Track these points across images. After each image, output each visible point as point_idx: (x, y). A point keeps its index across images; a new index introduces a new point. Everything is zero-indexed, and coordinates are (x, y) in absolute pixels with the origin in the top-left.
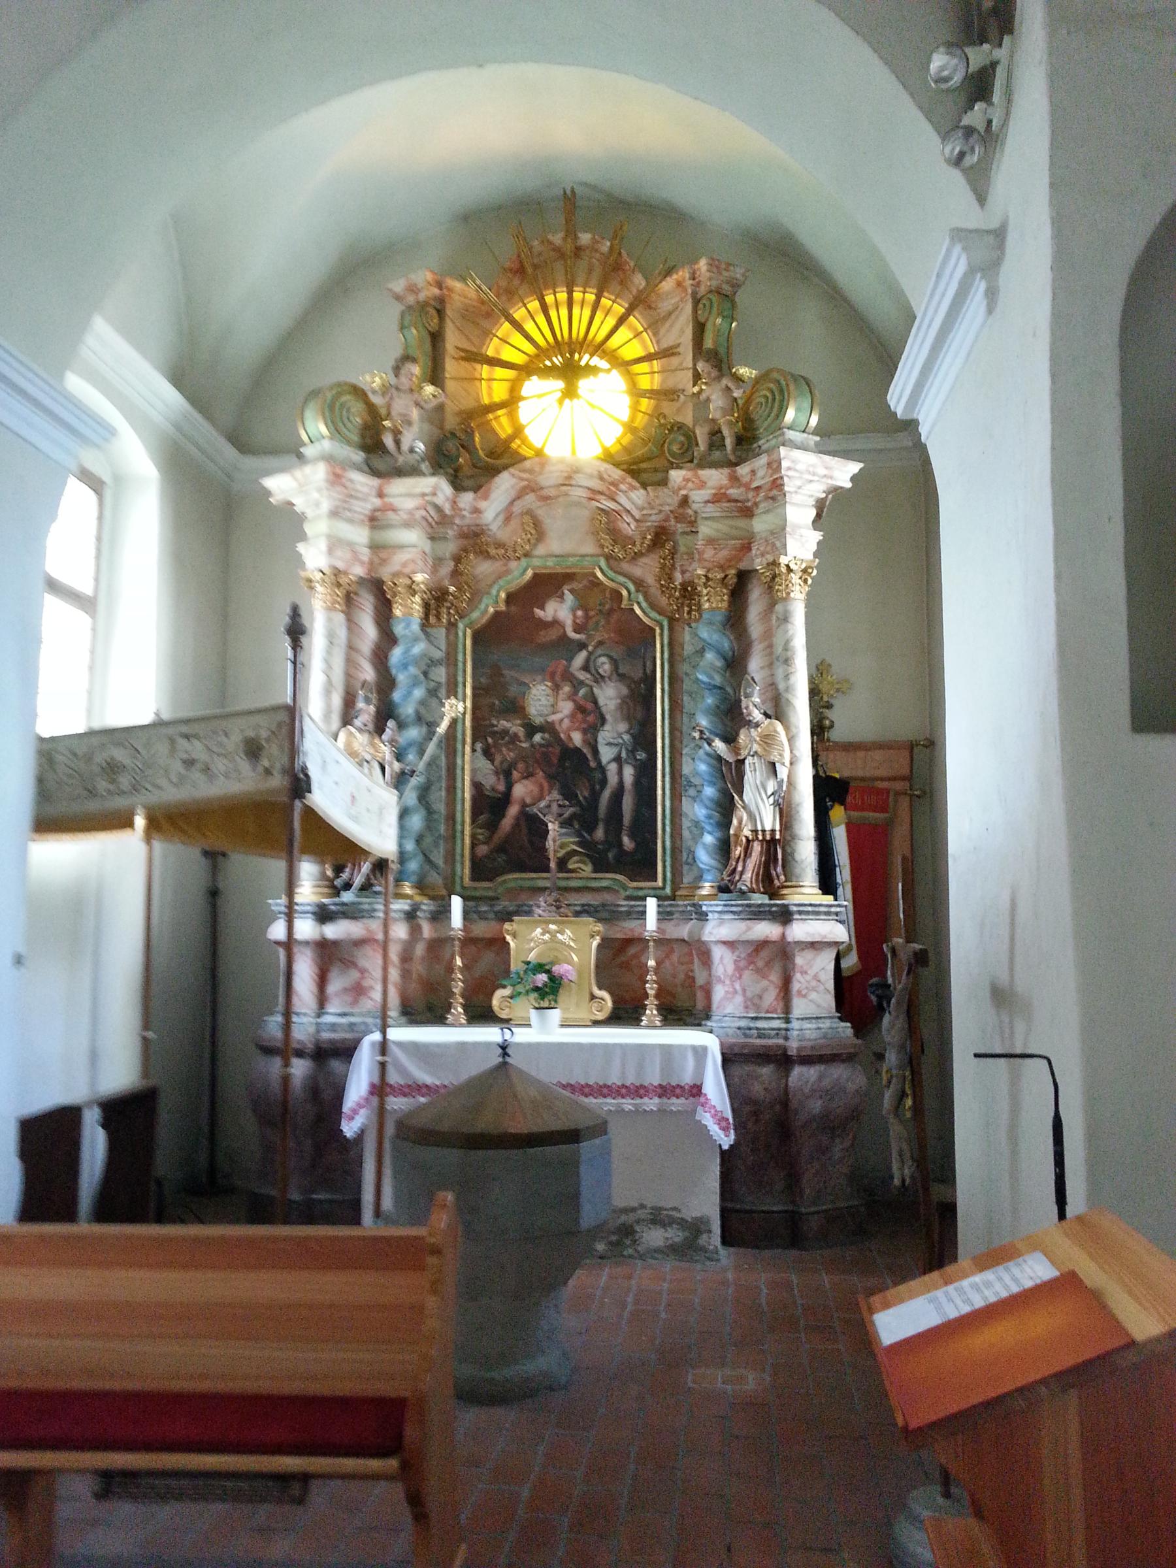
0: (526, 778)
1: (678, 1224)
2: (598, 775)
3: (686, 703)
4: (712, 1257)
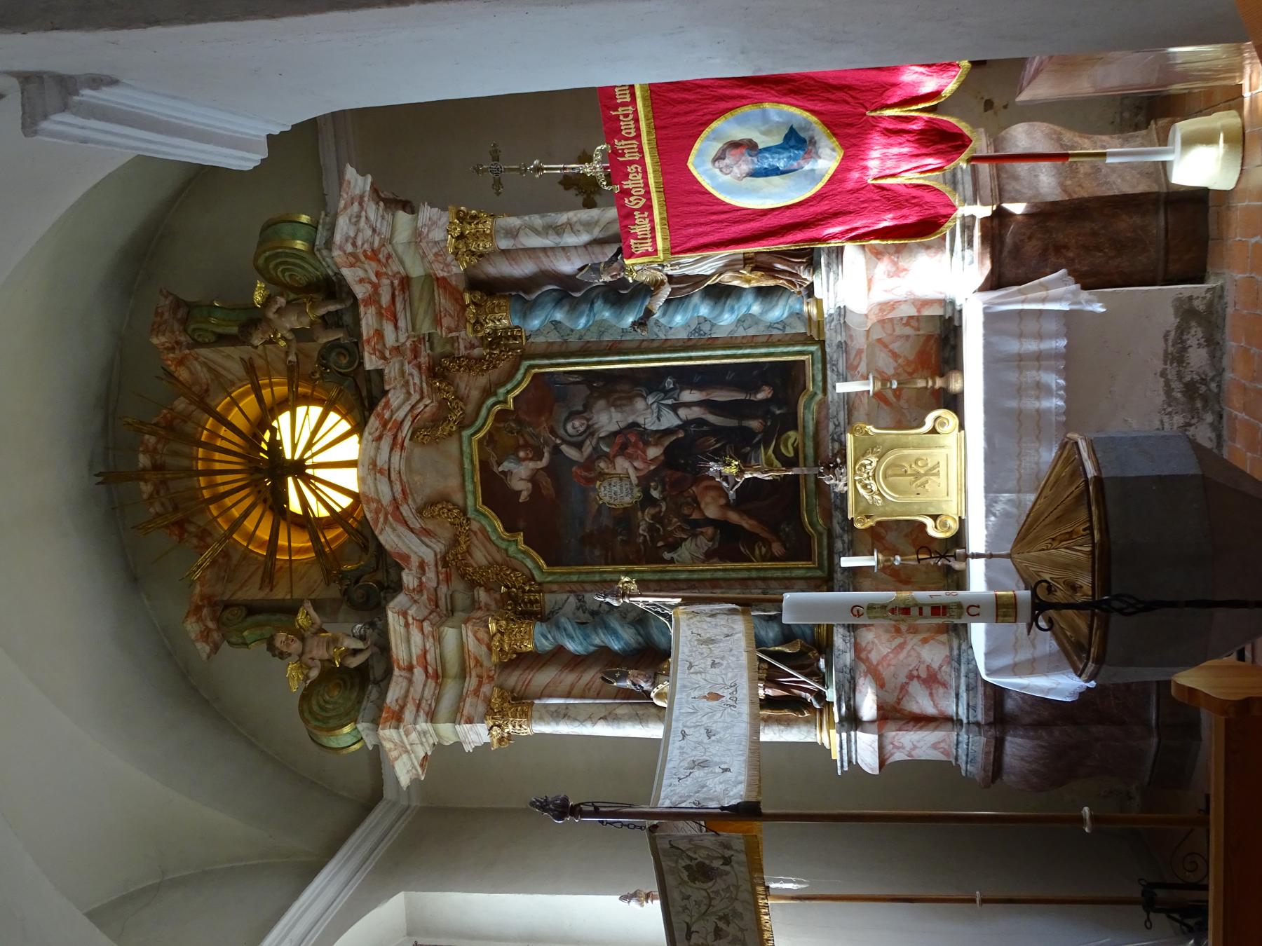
0: (699, 505)
1: (1182, 333)
2: (692, 428)
3: (611, 338)
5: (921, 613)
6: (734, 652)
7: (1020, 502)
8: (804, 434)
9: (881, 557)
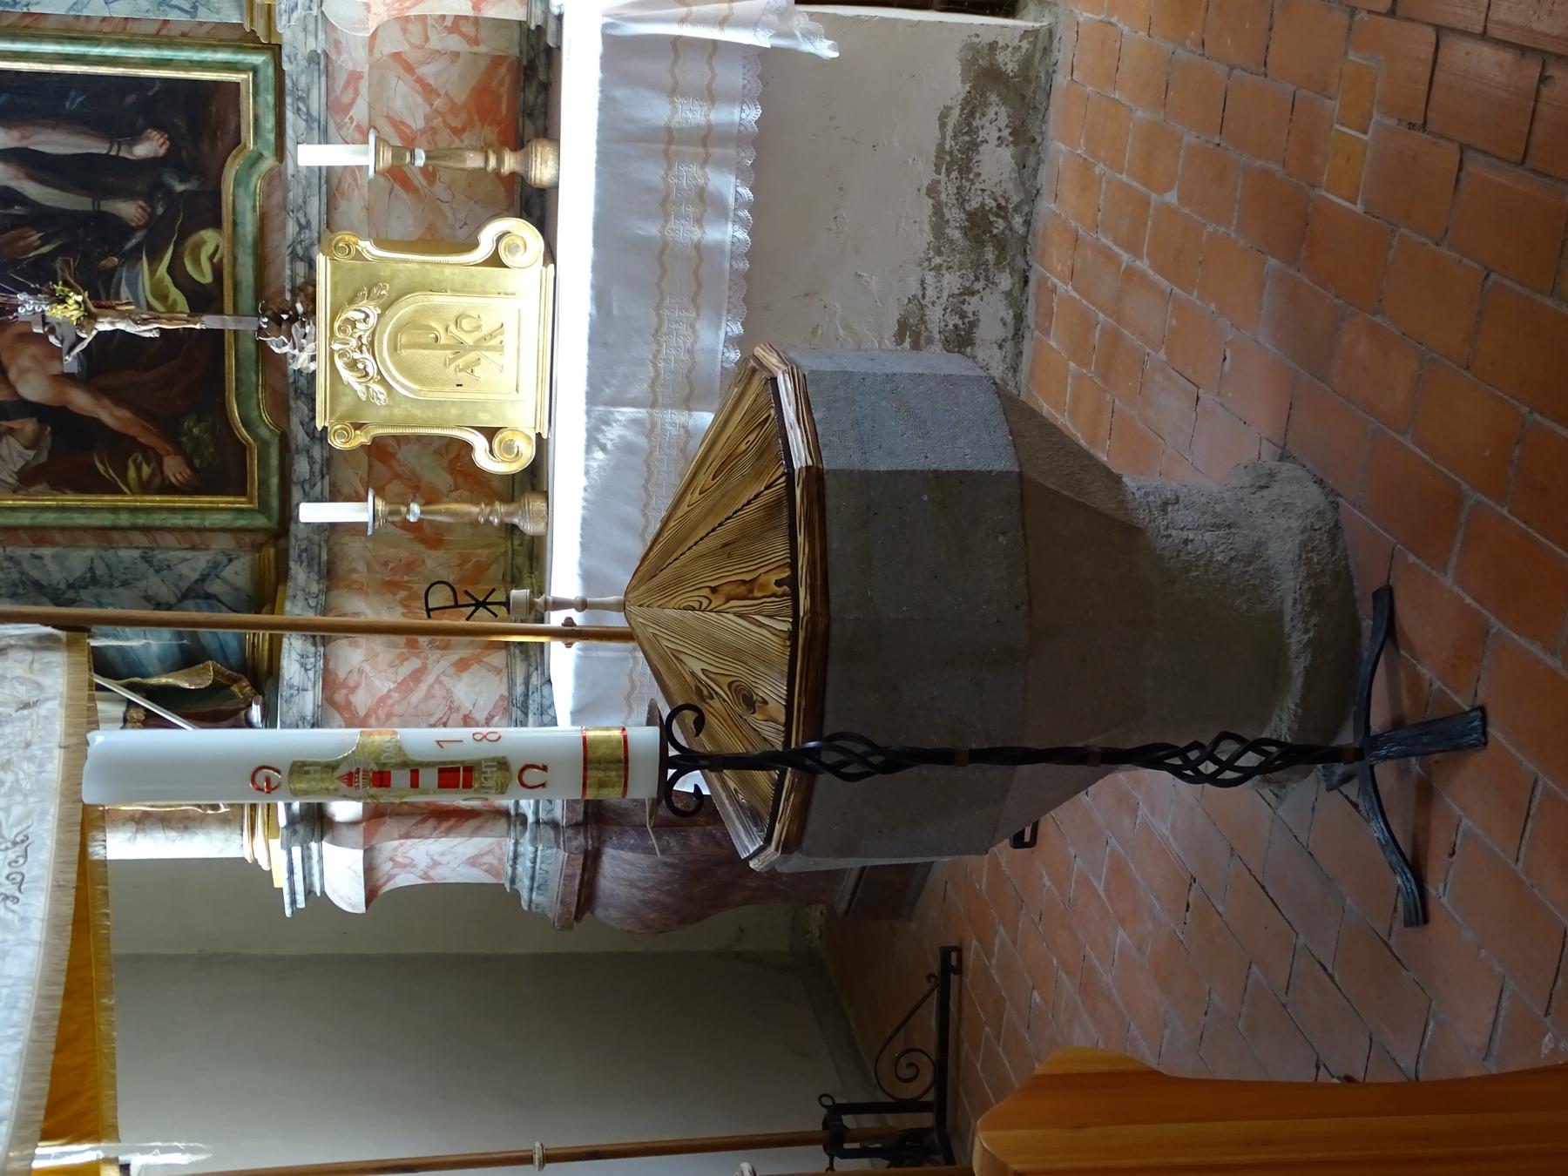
1: (972, 114)
4: (1043, 43)
5: (415, 784)
6: (36, 750)
7: (653, 425)
8: (235, 239)
9: (380, 505)
